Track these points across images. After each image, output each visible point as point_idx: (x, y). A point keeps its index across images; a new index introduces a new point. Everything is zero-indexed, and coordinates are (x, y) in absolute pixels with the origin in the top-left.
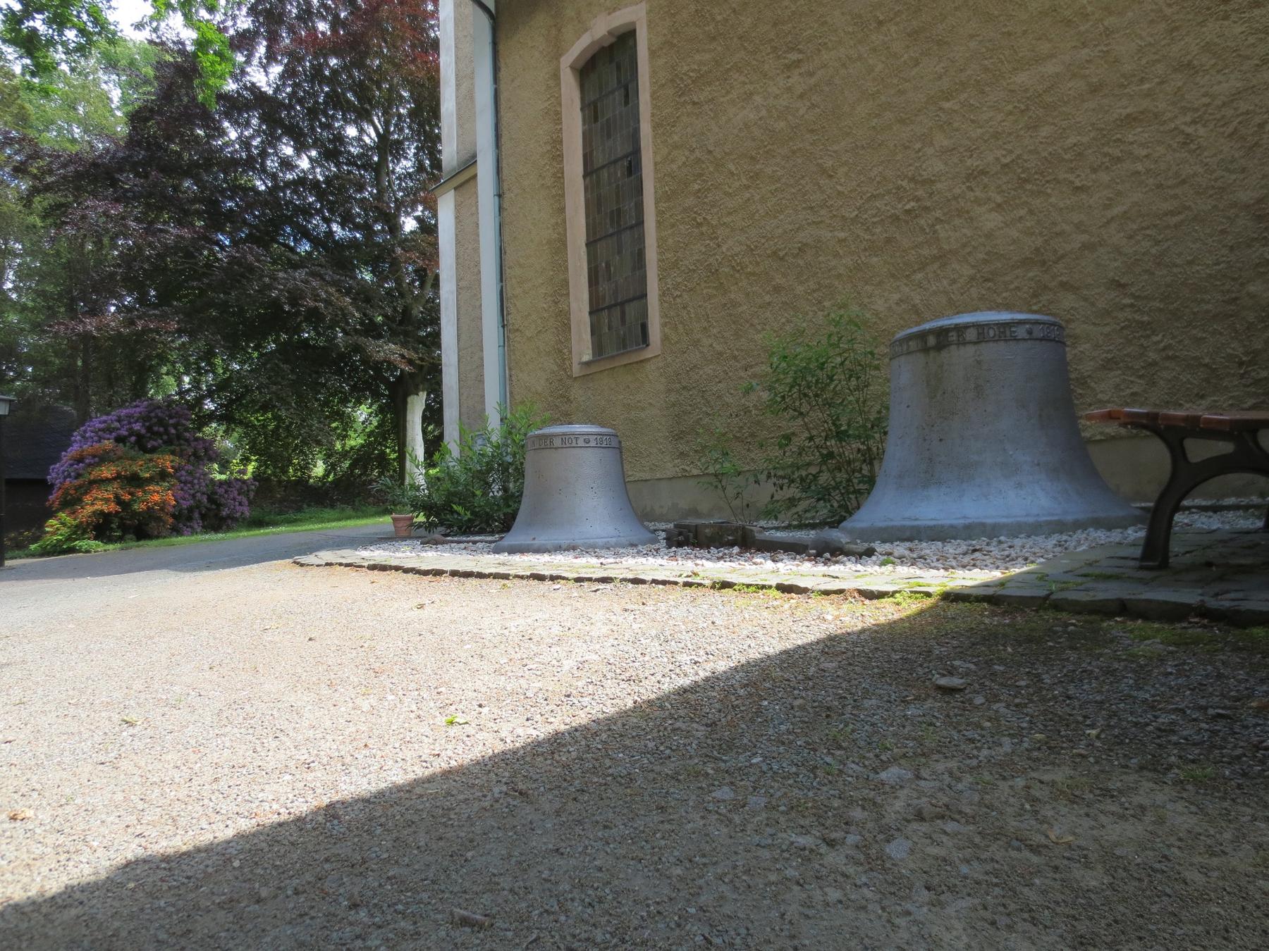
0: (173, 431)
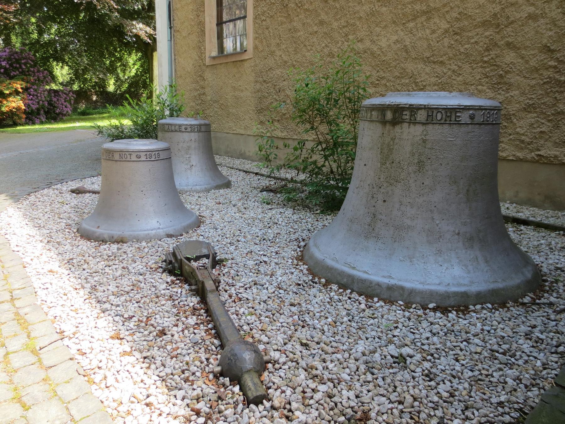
0: (24, 67)
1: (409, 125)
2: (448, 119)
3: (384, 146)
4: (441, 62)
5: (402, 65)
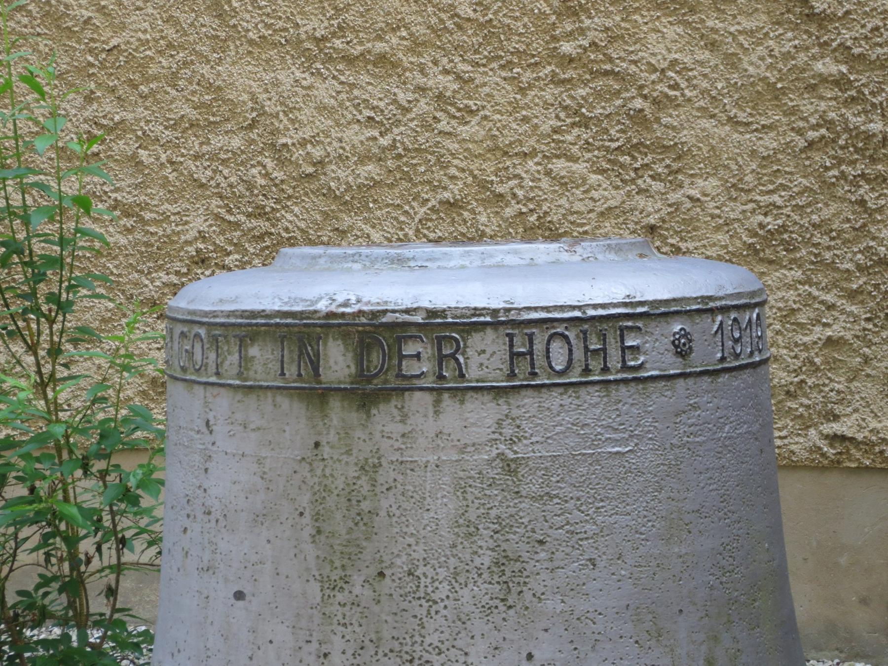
1: (437, 402)
2: (595, 364)
3: (331, 502)
4: (382, 59)
5: (205, 70)
